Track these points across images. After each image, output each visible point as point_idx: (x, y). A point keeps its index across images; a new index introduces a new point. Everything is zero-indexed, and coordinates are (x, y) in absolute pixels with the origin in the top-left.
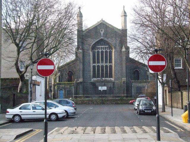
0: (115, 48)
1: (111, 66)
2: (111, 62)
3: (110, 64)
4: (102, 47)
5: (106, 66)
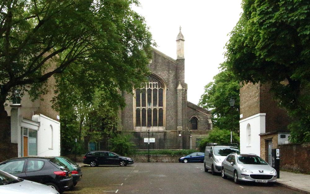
0: (167, 85)
1: (161, 110)
2: (161, 104)
4: (150, 83)
5: (155, 110)
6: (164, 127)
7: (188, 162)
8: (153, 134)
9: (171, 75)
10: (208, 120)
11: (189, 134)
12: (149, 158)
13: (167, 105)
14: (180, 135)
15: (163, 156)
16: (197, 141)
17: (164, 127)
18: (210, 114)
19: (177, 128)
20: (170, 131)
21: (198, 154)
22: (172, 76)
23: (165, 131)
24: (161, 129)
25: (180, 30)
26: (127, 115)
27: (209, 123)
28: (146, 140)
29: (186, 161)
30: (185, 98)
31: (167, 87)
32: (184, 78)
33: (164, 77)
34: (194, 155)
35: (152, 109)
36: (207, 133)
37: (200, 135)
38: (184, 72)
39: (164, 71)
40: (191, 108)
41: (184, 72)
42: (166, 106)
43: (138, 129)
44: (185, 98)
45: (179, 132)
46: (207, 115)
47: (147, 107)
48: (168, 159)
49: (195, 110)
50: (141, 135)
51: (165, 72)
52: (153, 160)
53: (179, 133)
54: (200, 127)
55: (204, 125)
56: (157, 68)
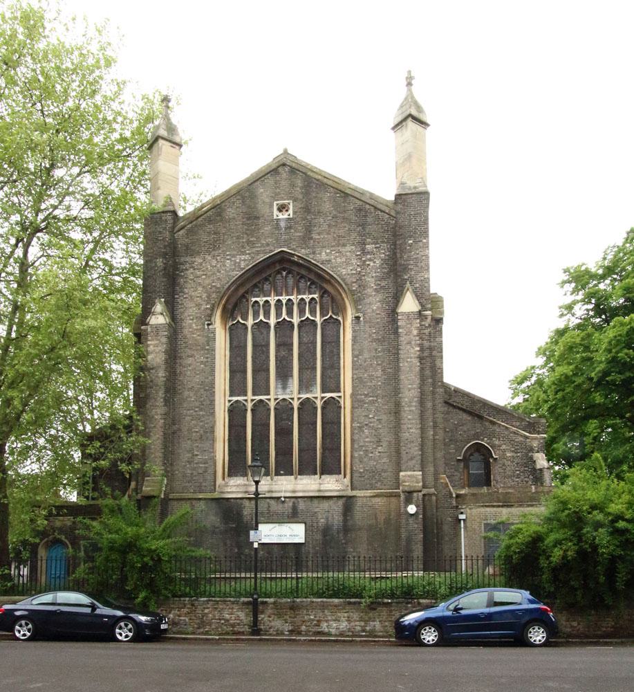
0: (357, 302)
1: (332, 407)
2: (331, 383)
3: (328, 395)
4: (284, 299)
5: (307, 405)
6: (345, 477)
7: (442, 642)
8: (295, 508)
9: (370, 260)
10: (531, 458)
11: (454, 503)
12: (255, 614)
13: (357, 381)
14: (412, 509)
15: (323, 607)
16: (491, 534)
17: (345, 477)
18: (539, 433)
19: (397, 478)
20: (369, 493)
21: (497, 600)
22: (376, 263)
23: (350, 493)
24: (331, 484)
25: (409, 84)
26: (189, 430)
27: (538, 467)
28: (268, 533)
29: (430, 636)
30: (434, 353)
31: (358, 310)
32: (428, 270)
33: (344, 272)
34: (474, 602)
35: (296, 404)
36: (533, 500)
37: (505, 510)
38: (428, 243)
39: (344, 245)
40: (464, 411)
41: (426, 246)
42: (354, 387)
43: (236, 487)
44: (434, 353)
45: (409, 496)
46: (527, 437)
47: (272, 396)
48: (349, 621)
49: (480, 417)
50: (245, 513)
51: (348, 248)
52: (277, 624)
53: (408, 501)
54: (502, 482)
55: (518, 476)
56: (315, 236)
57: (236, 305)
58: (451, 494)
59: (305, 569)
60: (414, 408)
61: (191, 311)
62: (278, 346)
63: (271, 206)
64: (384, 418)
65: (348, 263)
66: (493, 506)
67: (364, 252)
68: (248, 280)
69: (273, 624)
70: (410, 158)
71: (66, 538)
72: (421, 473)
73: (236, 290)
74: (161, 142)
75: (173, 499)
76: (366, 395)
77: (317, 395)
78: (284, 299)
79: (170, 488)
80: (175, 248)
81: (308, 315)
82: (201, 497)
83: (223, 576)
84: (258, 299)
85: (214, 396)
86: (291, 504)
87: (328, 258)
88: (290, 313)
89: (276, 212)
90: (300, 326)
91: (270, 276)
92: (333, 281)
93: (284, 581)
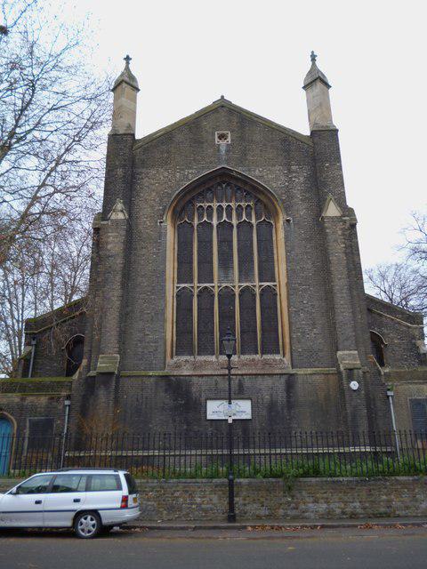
0: (287, 209)
1: (269, 295)
2: (267, 272)
3: (266, 284)
5: (227, 296)
8: (241, 385)
9: (295, 177)
13: (291, 273)
20: (309, 371)
22: (300, 179)
28: (216, 410)
33: (275, 185)
41: (340, 168)
43: (184, 365)
46: (409, 327)
47: (216, 284)
53: (351, 378)
57: (183, 209)
58: (380, 372)
59: (252, 446)
60: (345, 295)
61: (145, 211)
62: (220, 242)
63: (214, 135)
64: (316, 303)
65: (277, 179)
66: (416, 383)
67: (290, 171)
68: (194, 189)
69: (248, 508)
70: (319, 107)
71: (275, 360)
72: (356, 352)
73: (185, 195)
74: (124, 85)
75: (125, 376)
76: (300, 284)
77: (257, 285)
78: (224, 205)
79: (122, 367)
80: (133, 162)
81: (244, 218)
82: (151, 374)
83: (172, 453)
84: (202, 205)
85: (165, 282)
86: (237, 381)
87: (260, 174)
88: (229, 216)
89: (217, 139)
90: (238, 226)
91: (212, 187)
92: (266, 192)
93: (177, 458)
